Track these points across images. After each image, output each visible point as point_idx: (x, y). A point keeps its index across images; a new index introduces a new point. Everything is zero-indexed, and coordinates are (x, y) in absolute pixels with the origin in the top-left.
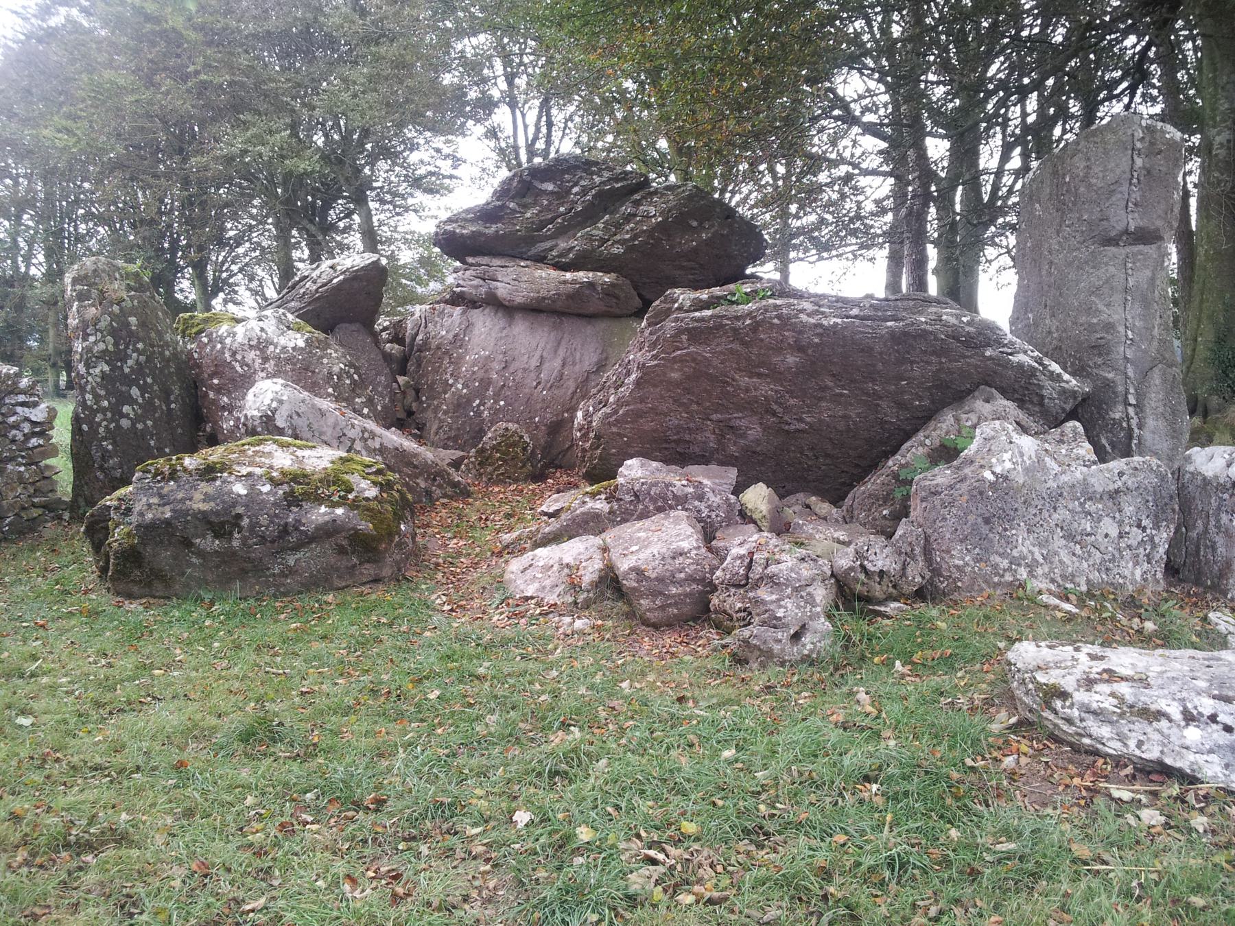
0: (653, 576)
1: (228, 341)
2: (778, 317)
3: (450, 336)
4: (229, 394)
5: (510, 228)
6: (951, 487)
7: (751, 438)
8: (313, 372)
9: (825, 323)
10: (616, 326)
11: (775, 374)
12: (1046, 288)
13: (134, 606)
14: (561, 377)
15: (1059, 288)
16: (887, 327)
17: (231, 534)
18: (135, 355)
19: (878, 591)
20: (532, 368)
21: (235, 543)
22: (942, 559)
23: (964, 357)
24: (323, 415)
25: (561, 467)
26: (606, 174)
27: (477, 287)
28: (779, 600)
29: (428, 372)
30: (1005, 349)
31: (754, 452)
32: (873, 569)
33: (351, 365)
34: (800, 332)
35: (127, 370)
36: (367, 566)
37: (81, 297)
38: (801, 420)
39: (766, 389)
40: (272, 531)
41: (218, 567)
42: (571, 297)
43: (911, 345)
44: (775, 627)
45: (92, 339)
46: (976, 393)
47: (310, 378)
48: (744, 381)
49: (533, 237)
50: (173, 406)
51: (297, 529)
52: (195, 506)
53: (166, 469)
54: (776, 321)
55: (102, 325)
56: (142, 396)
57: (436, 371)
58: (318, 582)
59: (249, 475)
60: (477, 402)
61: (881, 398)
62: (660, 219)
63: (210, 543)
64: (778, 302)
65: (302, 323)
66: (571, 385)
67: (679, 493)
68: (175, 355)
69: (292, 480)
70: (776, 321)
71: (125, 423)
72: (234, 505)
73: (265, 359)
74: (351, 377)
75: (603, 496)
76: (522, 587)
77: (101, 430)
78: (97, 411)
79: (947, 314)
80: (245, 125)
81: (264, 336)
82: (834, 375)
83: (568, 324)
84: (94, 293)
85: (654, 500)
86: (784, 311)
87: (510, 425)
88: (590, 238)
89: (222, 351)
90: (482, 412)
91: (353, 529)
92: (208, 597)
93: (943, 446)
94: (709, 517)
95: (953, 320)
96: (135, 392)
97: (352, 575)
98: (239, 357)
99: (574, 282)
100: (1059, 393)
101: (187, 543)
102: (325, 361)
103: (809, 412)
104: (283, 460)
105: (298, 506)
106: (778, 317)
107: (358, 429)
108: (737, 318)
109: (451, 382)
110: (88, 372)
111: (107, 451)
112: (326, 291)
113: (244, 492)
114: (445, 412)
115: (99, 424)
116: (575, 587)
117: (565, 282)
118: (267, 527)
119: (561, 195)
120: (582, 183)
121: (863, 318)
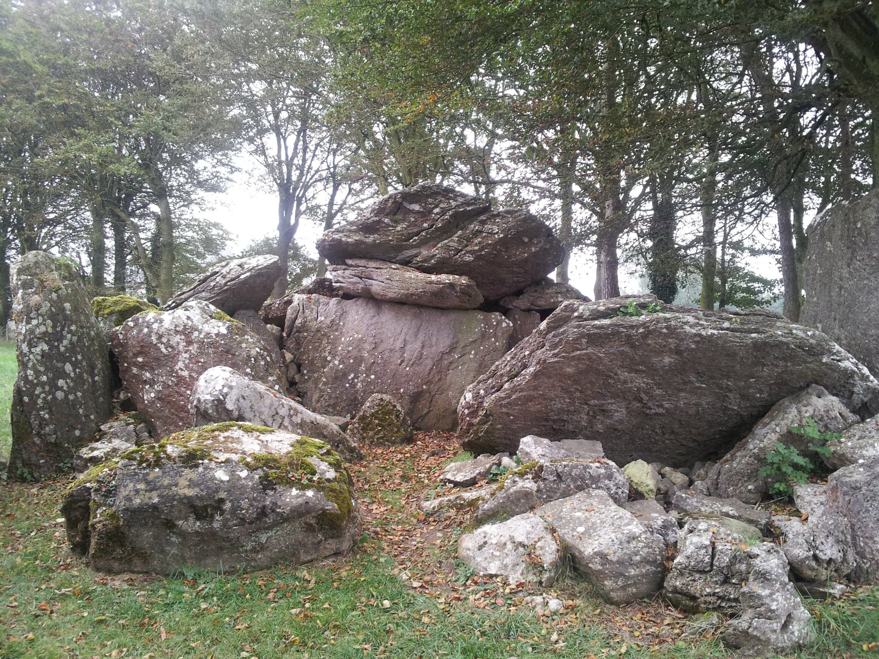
0: (615, 559)
2: (666, 327)
3: (328, 321)
4: (152, 370)
5: (384, 238)
6: (869, 484)
7: (616, 418)
8: (234, 355)
9: (704, 333)
10: (464, 317)
11: (651, 371)
12: (836, 305)
13: (118, 582)
14: (420, 357)
15: (849, 307)
16: (752, 338)
17: (212, 516)
18: (69, 336)
19: (824, 574)
21: (216, 525)
22: (866, 544)
23: (805, 362)
24: (262, 397)
25: (420, 430)
27: (355, 283)
28: (771, 594)
30: (835, 357)
31: (615, 430)
32: (824, 557)
33: (265, 349)
34: (682, 340)
35: (62, 349)
36: (330, 541)
37: (26, 285)
38: (661, 406)
39: (640, 382)
40: (252, 513)
41: (196, 545)
42: (435, 294)
43: (768, 353)
44: (770, 618)
45: (34, 322)
46: (810, 390)
48: (624, 375)
49: (401, 246)
50: (97, 378)
51: (273, 511)
52: (181, 492)
53: (151, 456)
54: (665, 331)
55: (43, 310)
56: (74, 371)
57: (316, 349)
58: (289, 558)
59: (228, 461)
60: (352, 375)
61: (730, 391)
62: (502, 236)
63: (191, 525)
64: (668, 315)
65: (222, 313)
66: (429, 363)
67: (594, 474)
68: (98, 334)
69: (265, 465)
70: (665, 331)
71: (60, 395)
73: (189, 343)
74: (264, 359)
75: (530, 476)
76: (484, 564)
77: (40, 401)
78: (37, 385)
79: (796, 329)
80: (79, 137)
81: (190, 323)
82: (698, 373)
83: (425, 313)
84: (36, 282)
85: (574, 480)
86: (673, 323)
87: (384, 396)
88: (447, 248)
90: (356, 384)
91: (322, 509)
92: (190, 574)
93: (789, 432)
94: (617, 493)
95: (801, 334)
96: (68, 367)
97: (317, 550)
98: (164, 340)
100: (864, 390)
101: (170, 525)
102: (244, 345)
103: (669, 400)
104: (251, 445)
105: (273, 489)
106: (666, 327)
107: (287, 407)
108: (632, 327)
109: (329, 358)
110: (30, 352)
111: (44, 419)
112: (234, 285)
113: (226, 478)
114: (325, 384)
115: (38, 396)
116: (536, 566)
117: (431, 283)
118: (247, 510)
119: (425, 214)
120: (442, 205)
121: (732, 330)
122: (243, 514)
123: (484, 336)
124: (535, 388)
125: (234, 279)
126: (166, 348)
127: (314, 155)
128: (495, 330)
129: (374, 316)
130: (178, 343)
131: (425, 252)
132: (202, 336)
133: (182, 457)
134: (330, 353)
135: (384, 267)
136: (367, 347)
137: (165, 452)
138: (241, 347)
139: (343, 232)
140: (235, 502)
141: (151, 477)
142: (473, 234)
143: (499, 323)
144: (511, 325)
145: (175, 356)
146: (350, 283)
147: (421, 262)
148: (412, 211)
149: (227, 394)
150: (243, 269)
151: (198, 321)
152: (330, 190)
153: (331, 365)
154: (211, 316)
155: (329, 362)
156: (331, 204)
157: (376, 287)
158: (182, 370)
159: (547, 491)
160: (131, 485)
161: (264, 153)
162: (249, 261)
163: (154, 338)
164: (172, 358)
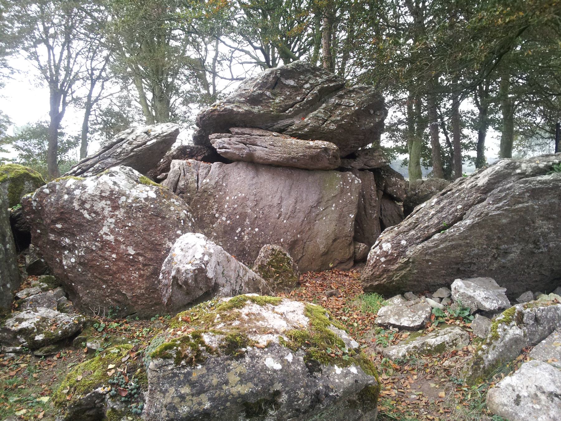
1: (77, 192)
3: (213, 183)
4: (72, 235)
8: (164, 218)
14: (294, 211)
20: (275, 204)
26: (325, 77)
27: (240, 149)
29: (197, 209)
47: (161, 222)
51: (327, 395)
52: (234, 390)
59: (270, 345)
60: (239, 229)
62: (357, 108)
66: (301, 216)
72: (272, 384)
73: (116, 207)
81: (117, 188)
83: (295, 174)
88: (316, 118)
89: (71, 201)
90: (243, 237)
98: (87, 206)
99: (316, 147)
102: (172, 208)
109: (217, 215)
112: (140, 151)
117: (310, 147)
119: (297, 89)
120: (311, 82)
122: (299, 405)
123: (342, 191)
124: (466, 238)
125: (139, 146)
126: (89, 214)
127: (75, 61)
128: (350, 187)
129: (254, 178)
130: (103, 209)
131: (297, 122)
132: (130, 201)
133: (223, 347)
134: (217, 210)
135: (267, 134)
136: (250, 204)
137: (203, 343)
138: (170, 210)
139: (233, 103)
140: (291, 393)
141: (195, 376)
142: (334, 107)
143: (353, 180)
144: (360, 182)
145: (97, 223)
146: (236, 148)
147: (297, 130)
148: (288, 86)
149: (207, 262)
150: (149, 135)
151: (125, 186)
152: (89, 86)
153: (219, 221)
154: (137, 181)
155: (217, 218)
156: (89, 96)
157: (260, 152)
158: (106, 234)
159: (530, 334)
160: (172, 390)
161: (37, 59)
162: (153, 129)
163: (76, 205)
164: (97, 223)
